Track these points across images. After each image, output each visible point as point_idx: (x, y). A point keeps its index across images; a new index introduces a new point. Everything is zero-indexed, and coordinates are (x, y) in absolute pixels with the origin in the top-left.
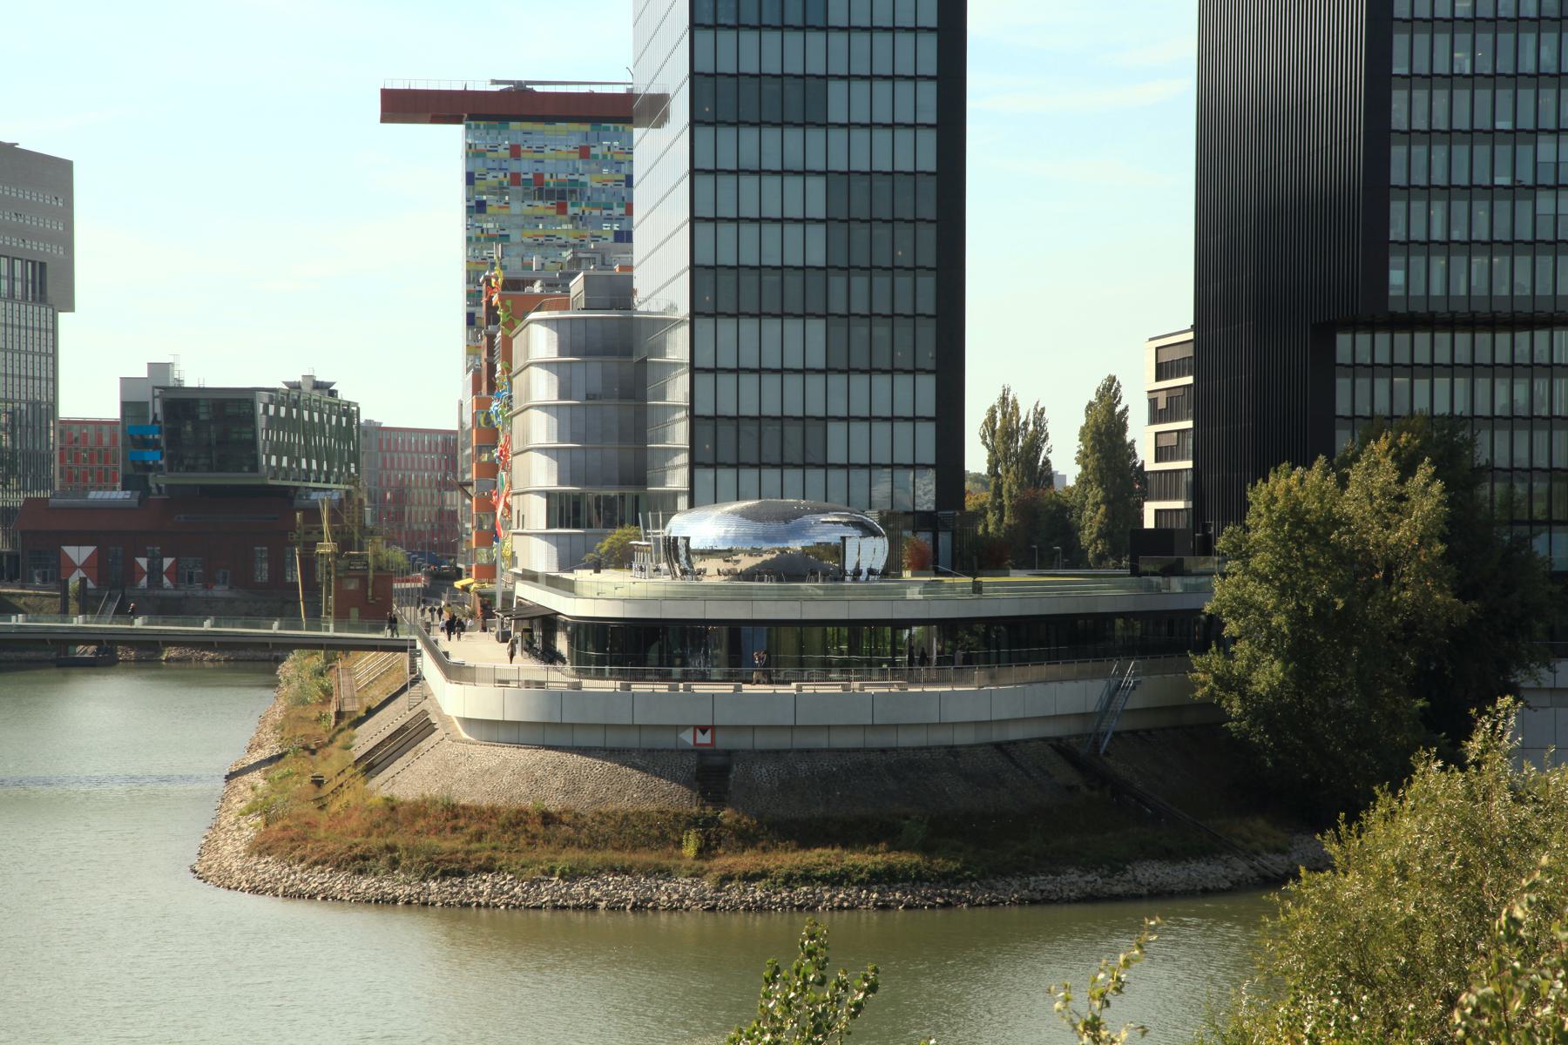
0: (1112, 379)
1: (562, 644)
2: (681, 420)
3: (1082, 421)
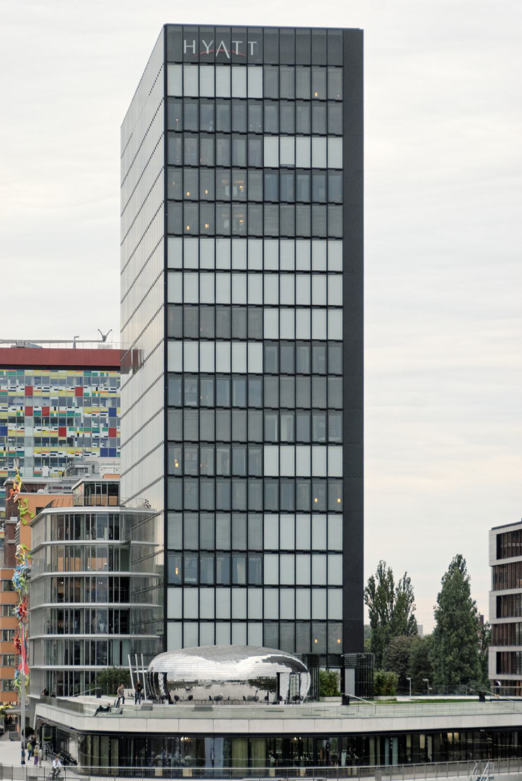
0: (460, 557)
1: (73, 749)
2: (160, 552)
3: (439, 588)
